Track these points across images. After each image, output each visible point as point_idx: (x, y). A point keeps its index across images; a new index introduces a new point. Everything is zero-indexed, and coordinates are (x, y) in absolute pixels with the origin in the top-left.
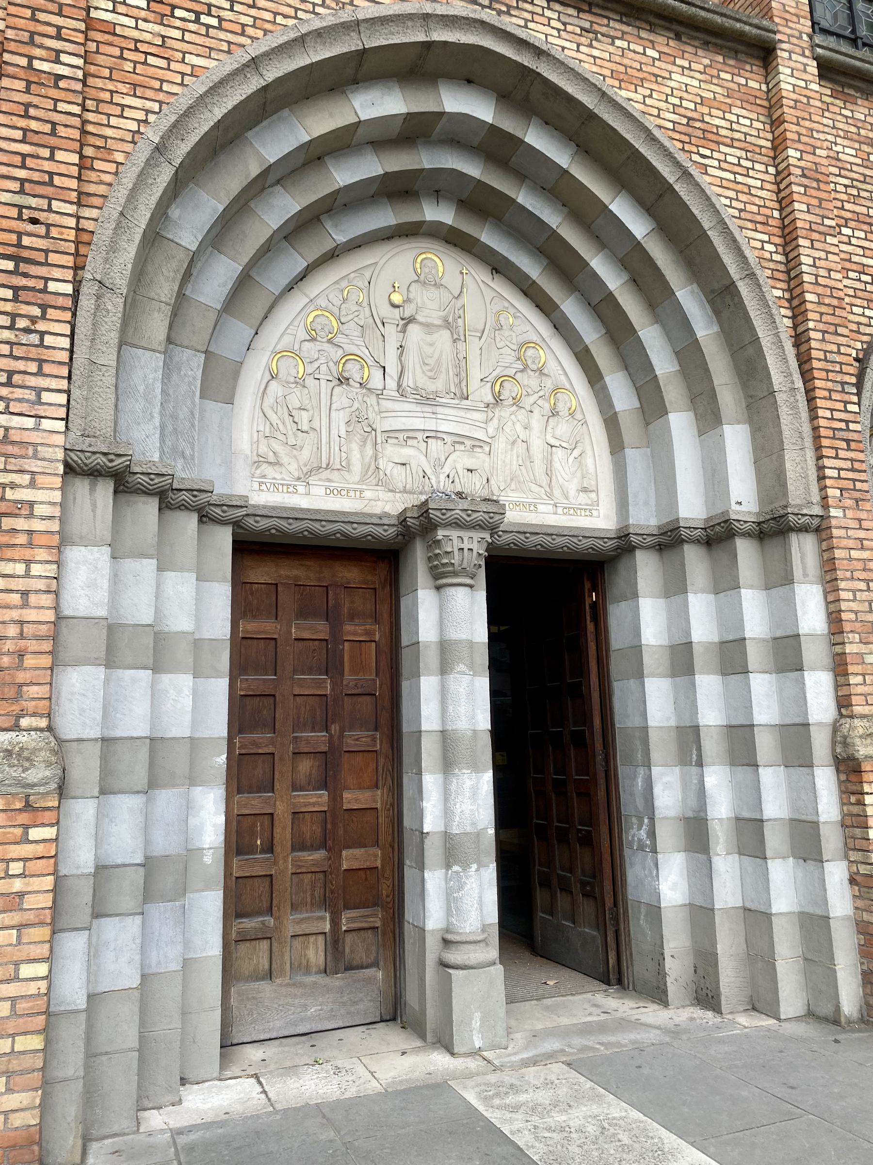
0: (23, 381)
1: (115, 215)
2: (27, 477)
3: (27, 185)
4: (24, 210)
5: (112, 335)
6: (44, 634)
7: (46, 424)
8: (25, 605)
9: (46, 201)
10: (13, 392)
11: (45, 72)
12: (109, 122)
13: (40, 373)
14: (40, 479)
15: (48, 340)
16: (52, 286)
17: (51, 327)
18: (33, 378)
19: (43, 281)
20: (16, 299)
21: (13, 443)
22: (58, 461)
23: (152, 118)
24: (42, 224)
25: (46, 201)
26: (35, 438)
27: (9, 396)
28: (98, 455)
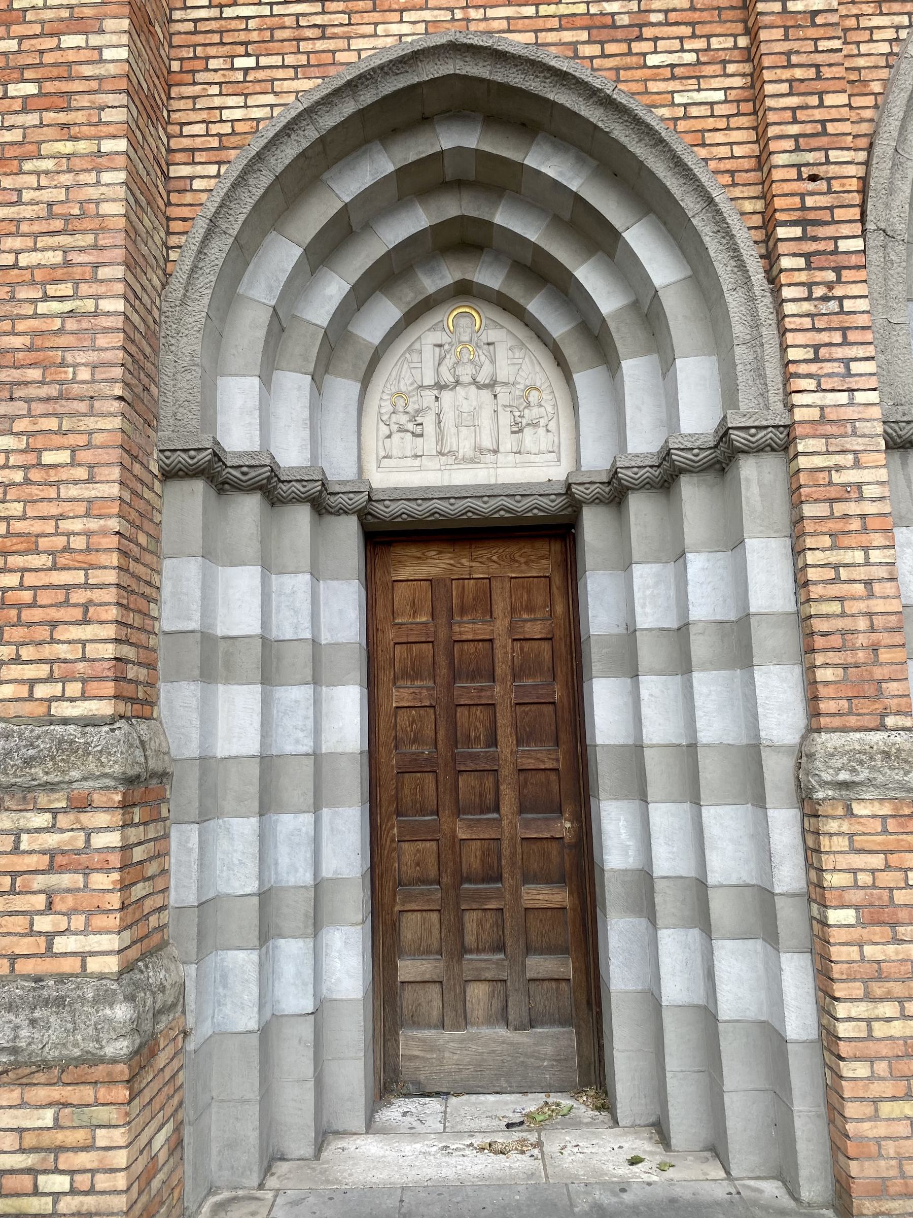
0: (830, 354)
1: (890, 151)
2: (850, 457)
3: (801, 140)
4: (803, 169)
5: (900, 288)
6: (894, 626)
7: (860, 397)
8: (871, 595)
9: (823, 153)
10: (821, 368)
11: (800, 12)
12: (859, 50)
13: (845, 343)
14: (864, 458)
15: (848, 305)
16: (843, 245)
17: (849, 290)
18: (839, 350)
19: (833, 241)
20: (809, 267)
21: (831, 422)
22: (879, 435)
23: (903, 34)
24: (822, 179)
25: (823, 153)
26: (850, 413)
27: (819, 372)
28: (178, 453)
